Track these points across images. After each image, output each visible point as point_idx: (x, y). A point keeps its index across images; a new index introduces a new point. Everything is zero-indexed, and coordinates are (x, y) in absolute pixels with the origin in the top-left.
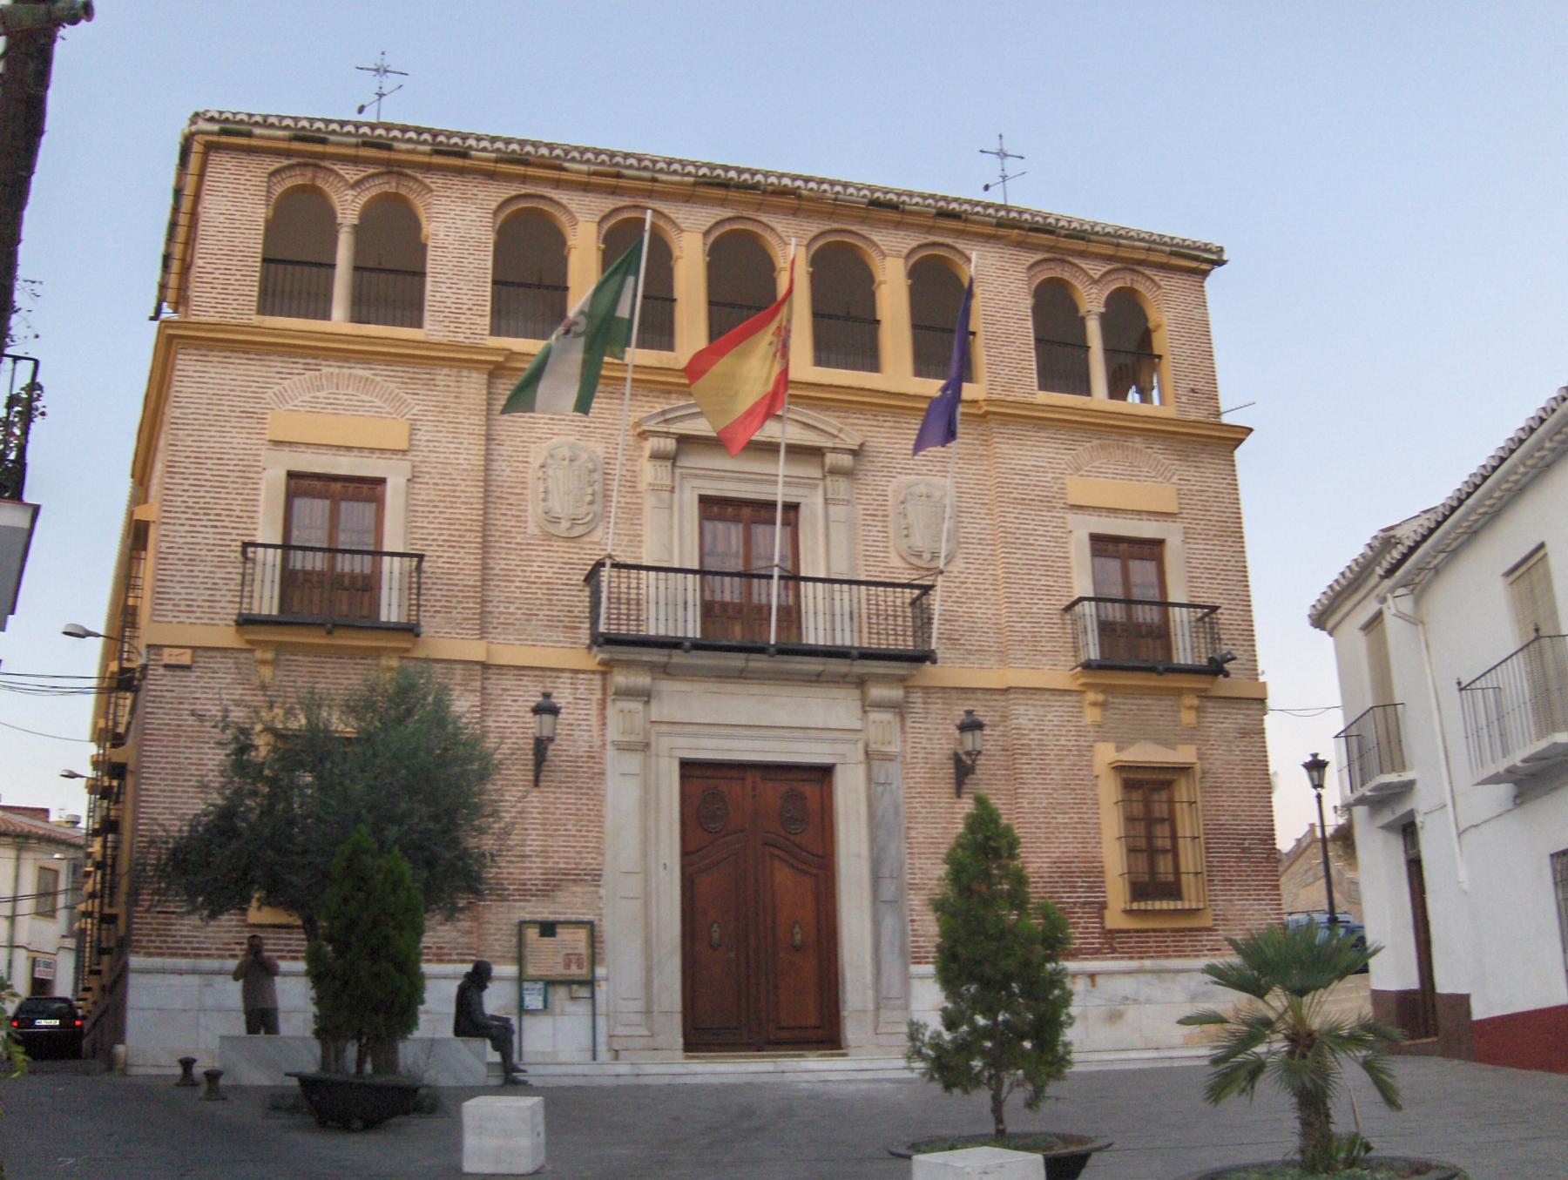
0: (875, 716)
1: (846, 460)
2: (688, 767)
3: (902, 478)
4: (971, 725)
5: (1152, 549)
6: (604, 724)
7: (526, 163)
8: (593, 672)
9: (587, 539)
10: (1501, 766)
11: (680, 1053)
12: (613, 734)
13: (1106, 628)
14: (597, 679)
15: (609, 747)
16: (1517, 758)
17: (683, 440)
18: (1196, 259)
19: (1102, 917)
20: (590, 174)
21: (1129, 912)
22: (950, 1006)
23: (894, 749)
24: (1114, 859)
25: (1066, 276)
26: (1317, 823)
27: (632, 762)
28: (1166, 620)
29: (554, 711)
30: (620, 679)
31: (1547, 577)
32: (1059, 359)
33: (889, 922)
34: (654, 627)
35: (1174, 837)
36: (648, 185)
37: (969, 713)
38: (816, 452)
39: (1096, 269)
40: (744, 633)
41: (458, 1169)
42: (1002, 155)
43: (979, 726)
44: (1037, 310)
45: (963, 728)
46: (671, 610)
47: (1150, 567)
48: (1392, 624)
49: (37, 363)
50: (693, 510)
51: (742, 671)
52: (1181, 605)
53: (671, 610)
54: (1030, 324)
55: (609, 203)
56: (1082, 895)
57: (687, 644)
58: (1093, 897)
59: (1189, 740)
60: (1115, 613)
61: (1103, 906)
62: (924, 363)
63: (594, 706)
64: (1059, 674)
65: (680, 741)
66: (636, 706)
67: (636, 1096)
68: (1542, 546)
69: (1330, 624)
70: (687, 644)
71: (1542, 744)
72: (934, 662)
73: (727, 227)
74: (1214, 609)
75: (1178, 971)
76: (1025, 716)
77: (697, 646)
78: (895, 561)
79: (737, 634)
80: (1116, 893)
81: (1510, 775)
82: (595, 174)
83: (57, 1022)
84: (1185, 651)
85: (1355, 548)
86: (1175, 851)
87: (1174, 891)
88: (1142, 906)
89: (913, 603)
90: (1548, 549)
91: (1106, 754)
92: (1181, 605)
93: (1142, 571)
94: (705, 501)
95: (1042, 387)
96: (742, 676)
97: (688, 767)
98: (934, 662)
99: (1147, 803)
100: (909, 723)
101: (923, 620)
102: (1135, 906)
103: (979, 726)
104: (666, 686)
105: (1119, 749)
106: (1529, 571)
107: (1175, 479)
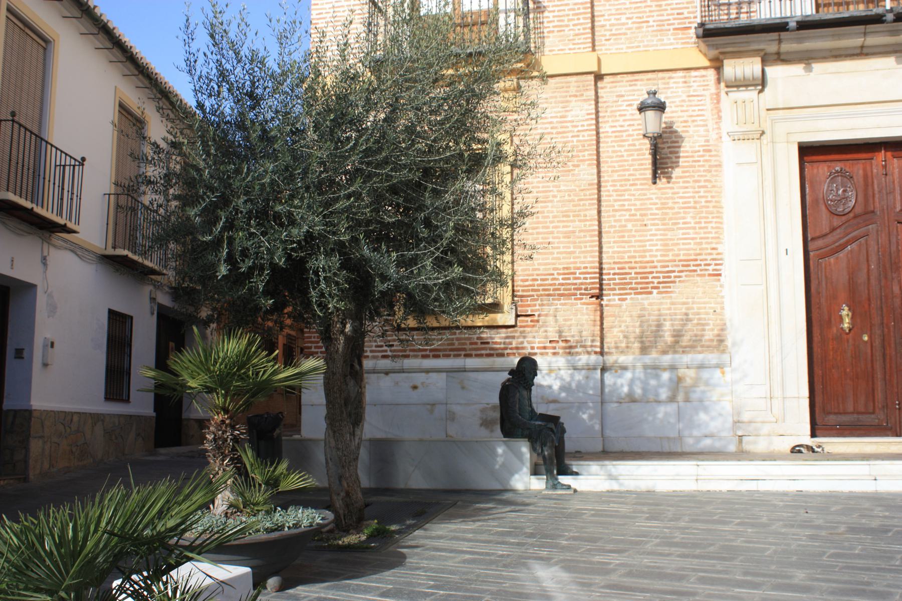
6: (720, 118)
8: (705, 68)
12: (728, 124)
14: (711, 74)
15: (725, 138)
22: (583, 382)
26: (136, 99)
27: (749, 150)
29: (660, 107)
30: (734, 68)
51: (862, 47)
57: (792, 25)
63: (708, 101)
66: (751, 94)
67: (97, 418)
70: (792, 25)
77: (805, 25)
83: (846, 325)
96: (862, 53)
104: (775, 72)
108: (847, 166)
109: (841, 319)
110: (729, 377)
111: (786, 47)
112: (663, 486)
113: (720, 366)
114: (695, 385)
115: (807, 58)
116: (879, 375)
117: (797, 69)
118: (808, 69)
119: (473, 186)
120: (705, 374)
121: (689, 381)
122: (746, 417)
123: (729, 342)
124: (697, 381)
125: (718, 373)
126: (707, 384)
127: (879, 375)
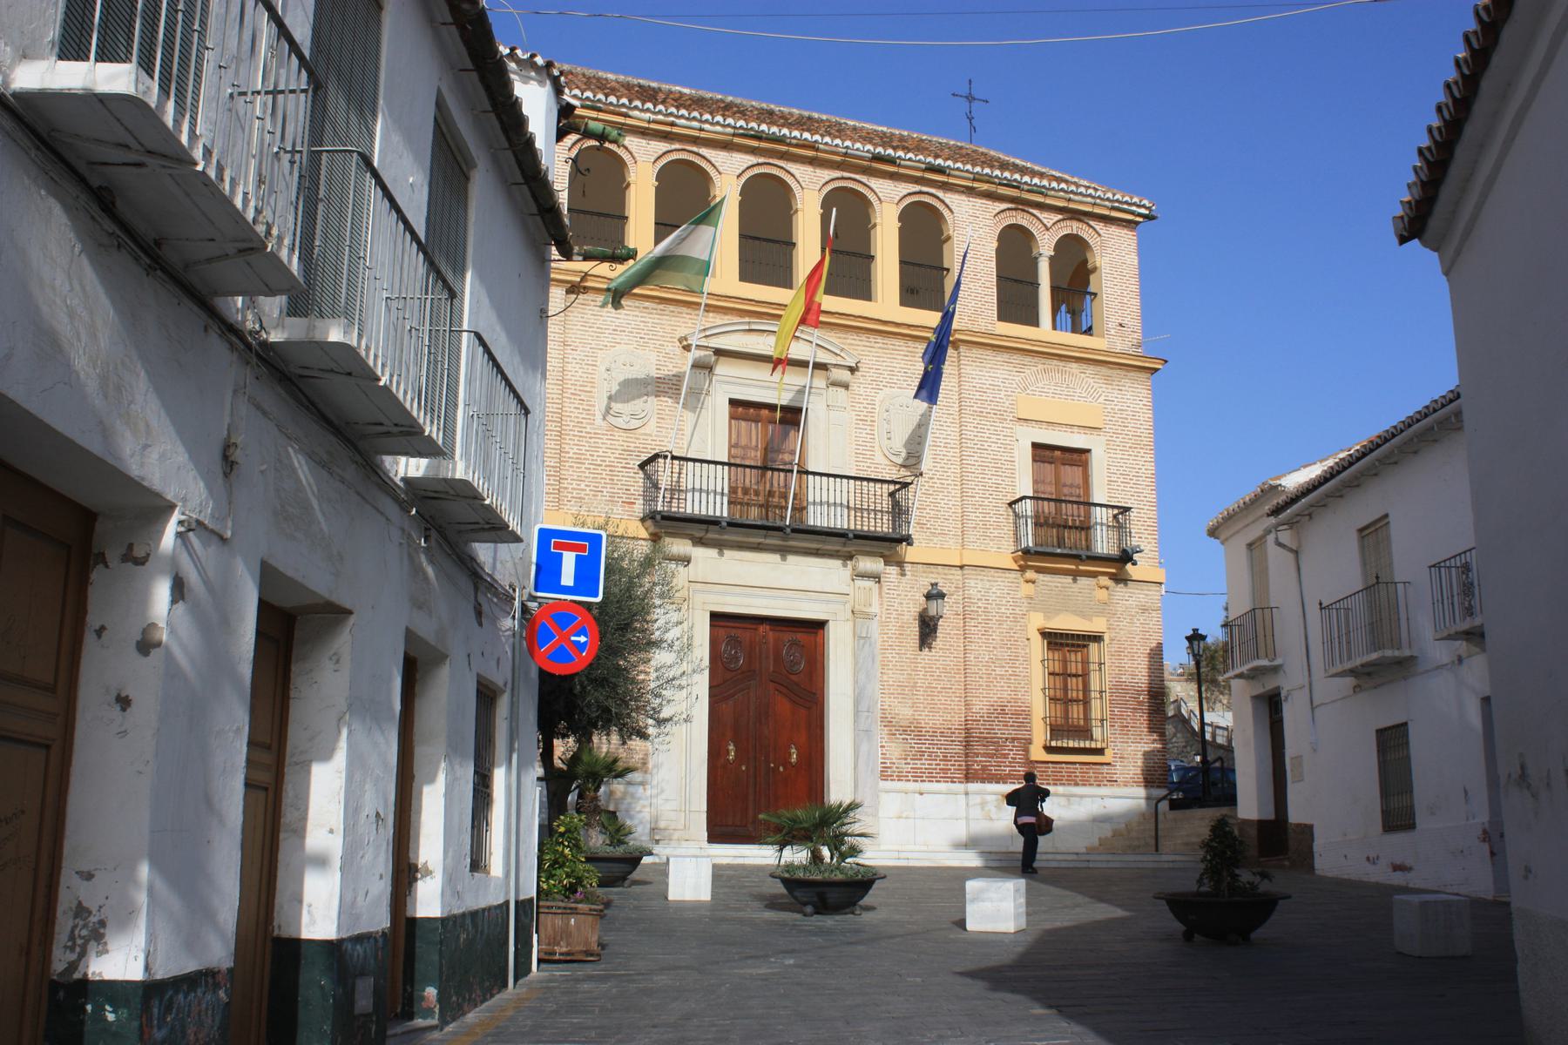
0: (861, 583)
1: (845, 375)
2: (716, 617)
3: (887, 390)
4: (934, 595)
5: (1078, 457)
7: (599, 110)
9: (641, 431)
10: (1348, 666)
11: (705, 844)
13: (1040, 522)
16: (1358, 661)
17: (719, 352)
18: (1132, 213)
19: (1027, 751)
20: (649, 122)
21: (1049, 749)
23: (875, 609)
24: (1039, 708)
25: (1024, 223)
28: (1088, 515)
31: (1388, 538)
32: (1016, 300)
33: (864, 748)
34: (693, 506)
35: (1086, 689)
36: (696, 133)
37: (934, 585)
38: (821, 367)
39: (1049, 218)
40: (766, 517)
41: (230, 971)
42: (970, 98)
43: (942, 596)
44: (1001, 253)
45: (929, 597)
46: (707, 494)
47: (1078, 471)
48: (1274, 555)
49: (642, 466)
50: (725, 408)
52: (1101, 505)
53: (707, 494)
54: (993, 264)
55: (663, 146)
56: (1012, 733)
58: (1022, 734)
59: (1101, 613)
60: (1049, 508)
61: (1030, 741)
62: (911, 294)
64: (1004, 554)
65: (711, 598)
68: (1386, 516)
69: (1223, 537)
71: (1374, 656)
72: (910, 544)
73: (757, 171)
74: (1128, 509)
75: (1082, 797)
76: (976, 586)
78: (879, 458)
79: (753, 515)
80: (1040, 735)
81: (1352, 672)
82: (655, 122)
84: (1104, 543)
85: (1248, 491)
86: (1086, 702)
87: (1085, 733)
88: (1059, 744)
89: (892, 495)
90: (1391, 519)
91: (1037, 621)
92: (1101, 505)
93: (1071, 474)
94: (734, 403)
95: (1000, 319)
96: (758, 548)
97: (716, 617)
98: (910, 544)
99: (1065, 662)
100: (885, 589)
101: (898, 511)
102: (1053, 744)
103: (942, 596)
105: (1047, 618)
106: (1373, 533)
107: (1101, 400)
108: (738, 633)
109: (728, 752)
110: (648, 793)
111: (710, 535)
112: (103, 87)
113: (642, 784)
114: (623, 798)
115: (721, 546)
116: (751, 798)
117: (713, 552)
118: (784, 558)
119: (618, 786)
120: (631, 789)
121: (618, 795)
122: (662, 824)
123: (650, 766)
124: (625, 793)
125: (641, 789)
126: (633, 796)
127: (751, 798)
